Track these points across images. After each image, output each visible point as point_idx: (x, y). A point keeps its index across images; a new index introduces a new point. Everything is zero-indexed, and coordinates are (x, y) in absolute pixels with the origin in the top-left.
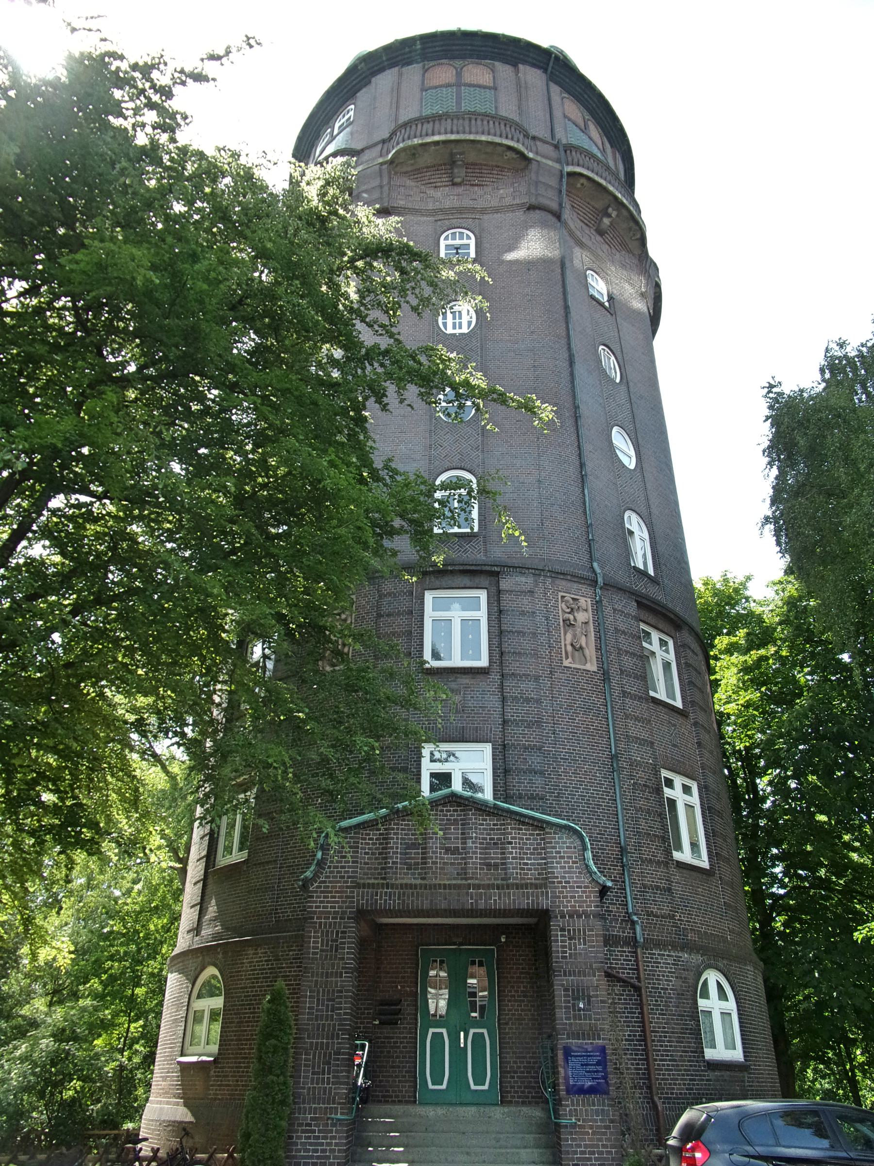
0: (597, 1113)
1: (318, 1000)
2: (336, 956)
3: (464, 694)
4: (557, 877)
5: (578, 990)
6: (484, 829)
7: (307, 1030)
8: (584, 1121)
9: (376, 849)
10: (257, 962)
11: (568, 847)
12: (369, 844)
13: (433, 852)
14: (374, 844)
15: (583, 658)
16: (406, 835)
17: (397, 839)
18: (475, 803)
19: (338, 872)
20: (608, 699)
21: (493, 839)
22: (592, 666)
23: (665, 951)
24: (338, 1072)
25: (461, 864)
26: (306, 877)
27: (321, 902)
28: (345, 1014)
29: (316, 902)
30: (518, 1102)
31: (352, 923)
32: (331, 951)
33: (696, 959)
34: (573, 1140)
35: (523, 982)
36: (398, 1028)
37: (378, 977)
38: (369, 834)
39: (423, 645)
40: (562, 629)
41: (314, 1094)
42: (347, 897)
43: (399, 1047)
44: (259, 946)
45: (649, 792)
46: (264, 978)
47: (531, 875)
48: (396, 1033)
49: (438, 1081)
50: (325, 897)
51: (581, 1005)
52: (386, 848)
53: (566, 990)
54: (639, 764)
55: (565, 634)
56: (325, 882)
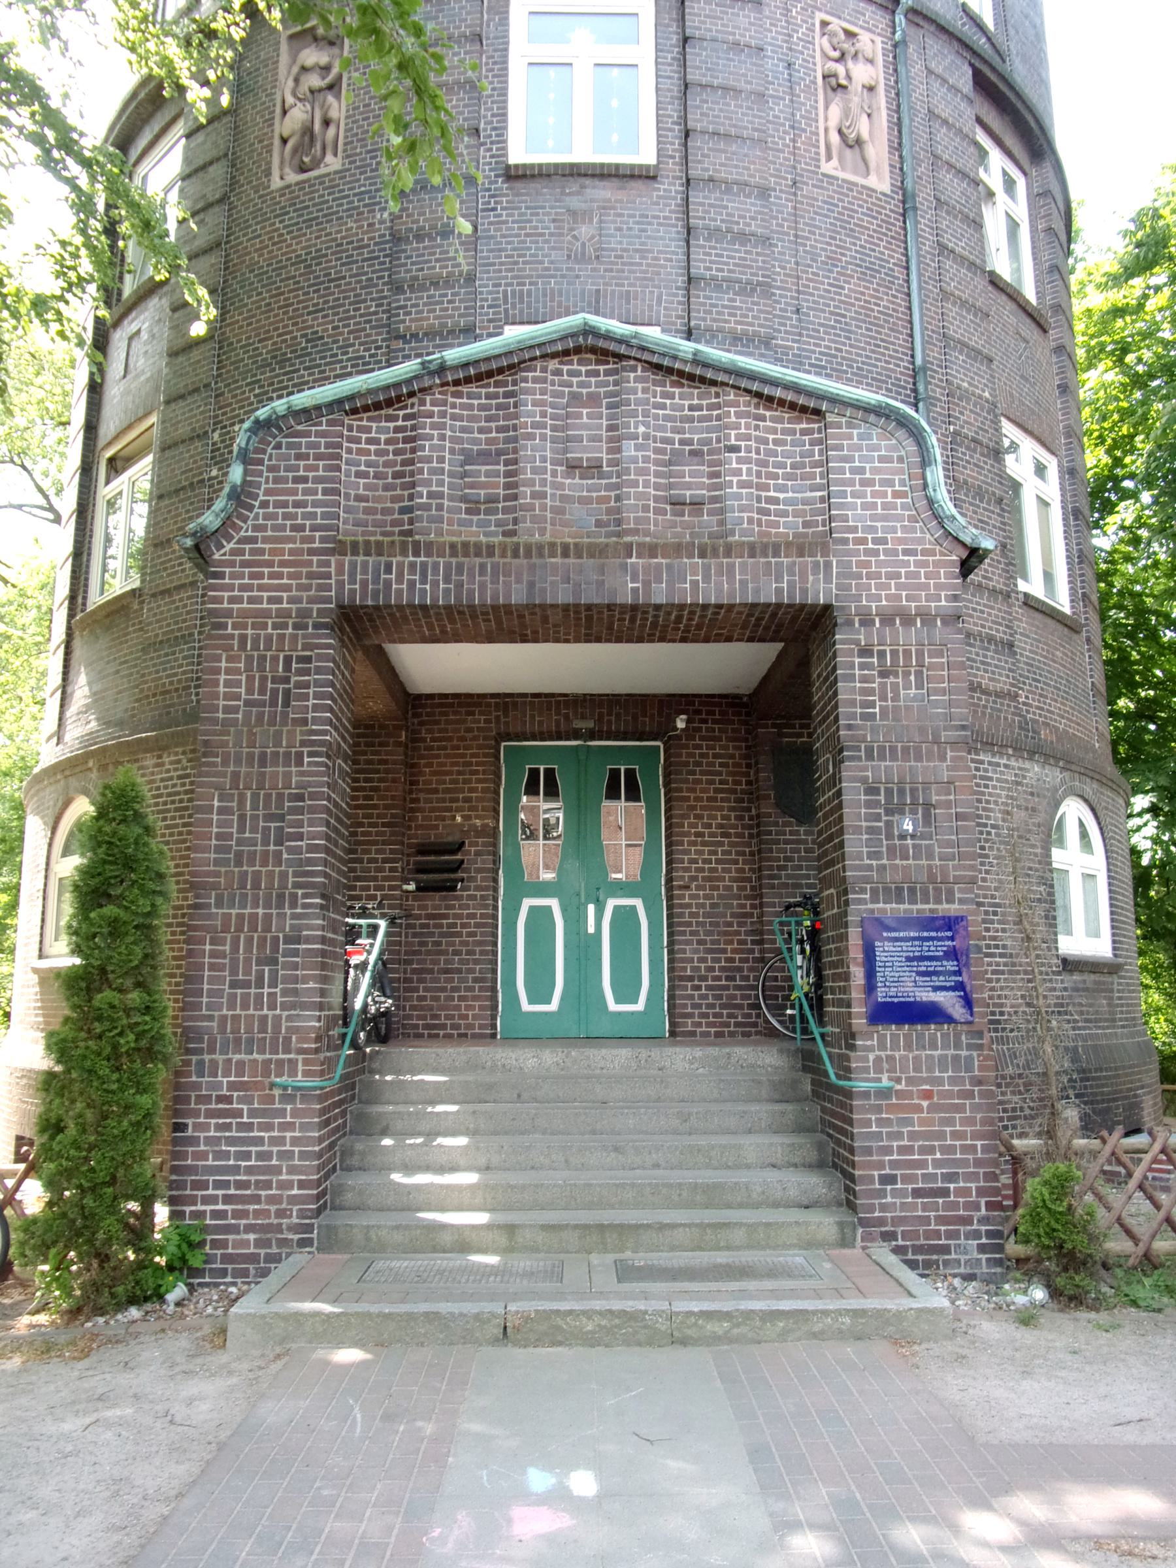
0: (943, 1063)
1: (242, 818)
2: (285, 715)
3: (601, 221)
4: (854, 529)
5: (901, 792)
6: (667, 418)
7: (215, 886)
8: (910, 1081)
9: (387, 464)
10: (162, 780)
11: (882, 459)
12: (367, 452)
13: (535, 471)
14: (378, 453)
15: (861, 164)
16: (463, 430)
17: (442, 438)
18: (643, 349)
19: (286, 516)
20: (912, 252)
21: (690, 442)
22: (881, 182)
23: (1001, 757)
24: (295, 979)
25: (606, 499)
26: (203, 528)
27: (243, 588)
28: (312, 848)
29: (231, 588)
30: (708, 1034)
31: (326, 636)
32: (274, 703)
33: (1053, 776)
34: (880, 1122)
35: (721, 809)
36: (456, 898)
37: (414, 801)
38: (368, 430)
39: (505, 115)
40: (821, 91)
41: (236, 1031)
42: (311, 576)
43: (459, 934)
44: (164, 749)
45: (982, 455)
46: (176, 810)
47: (786, 527)
48: (452, 907)
49: (540, 993)
50: (253, 576)
51: (908, 826)
52: (411, 462)
53: (872, 790)
54: (965, 396)
55: (827, 107)
56: (253, 540)
